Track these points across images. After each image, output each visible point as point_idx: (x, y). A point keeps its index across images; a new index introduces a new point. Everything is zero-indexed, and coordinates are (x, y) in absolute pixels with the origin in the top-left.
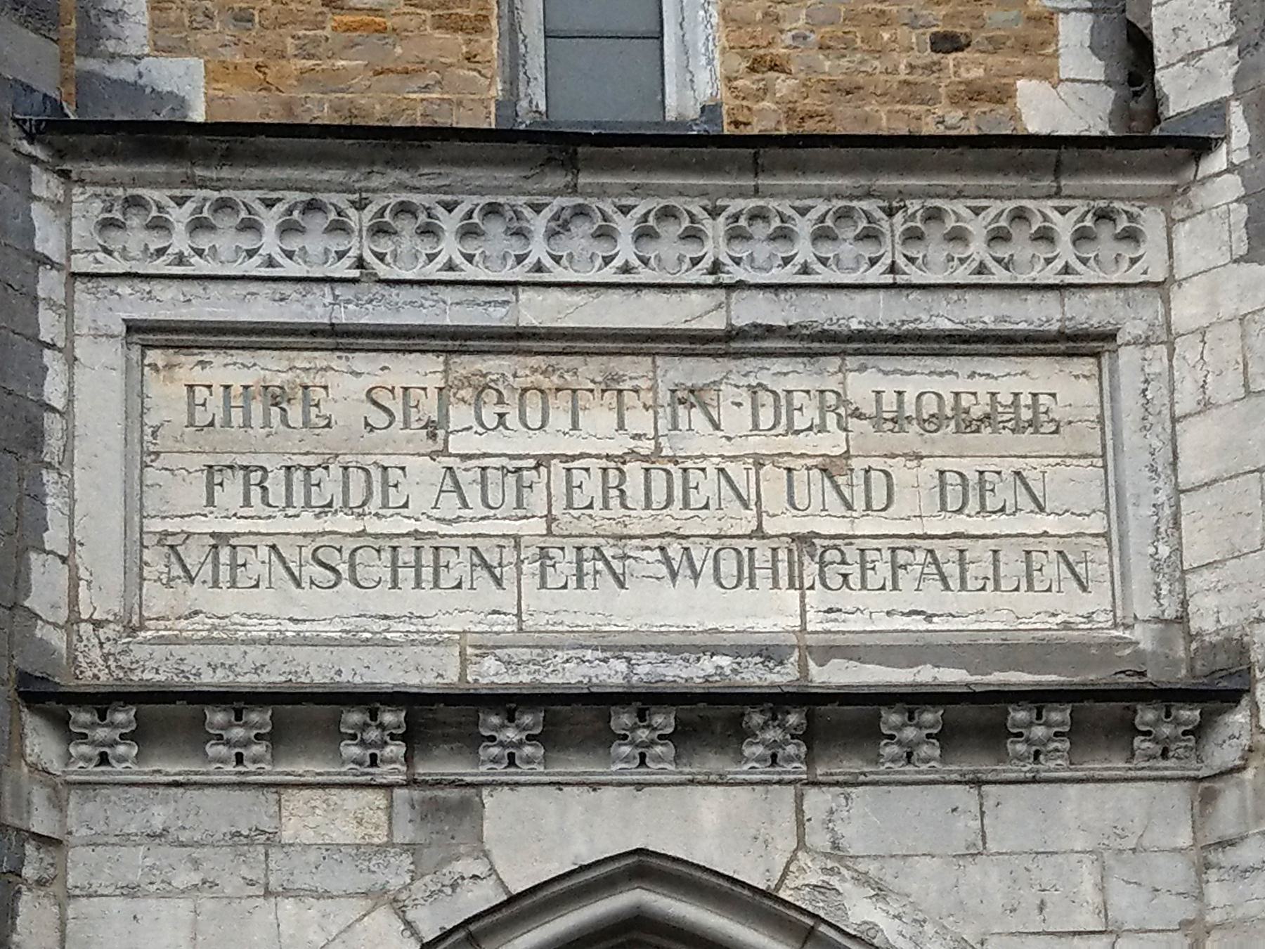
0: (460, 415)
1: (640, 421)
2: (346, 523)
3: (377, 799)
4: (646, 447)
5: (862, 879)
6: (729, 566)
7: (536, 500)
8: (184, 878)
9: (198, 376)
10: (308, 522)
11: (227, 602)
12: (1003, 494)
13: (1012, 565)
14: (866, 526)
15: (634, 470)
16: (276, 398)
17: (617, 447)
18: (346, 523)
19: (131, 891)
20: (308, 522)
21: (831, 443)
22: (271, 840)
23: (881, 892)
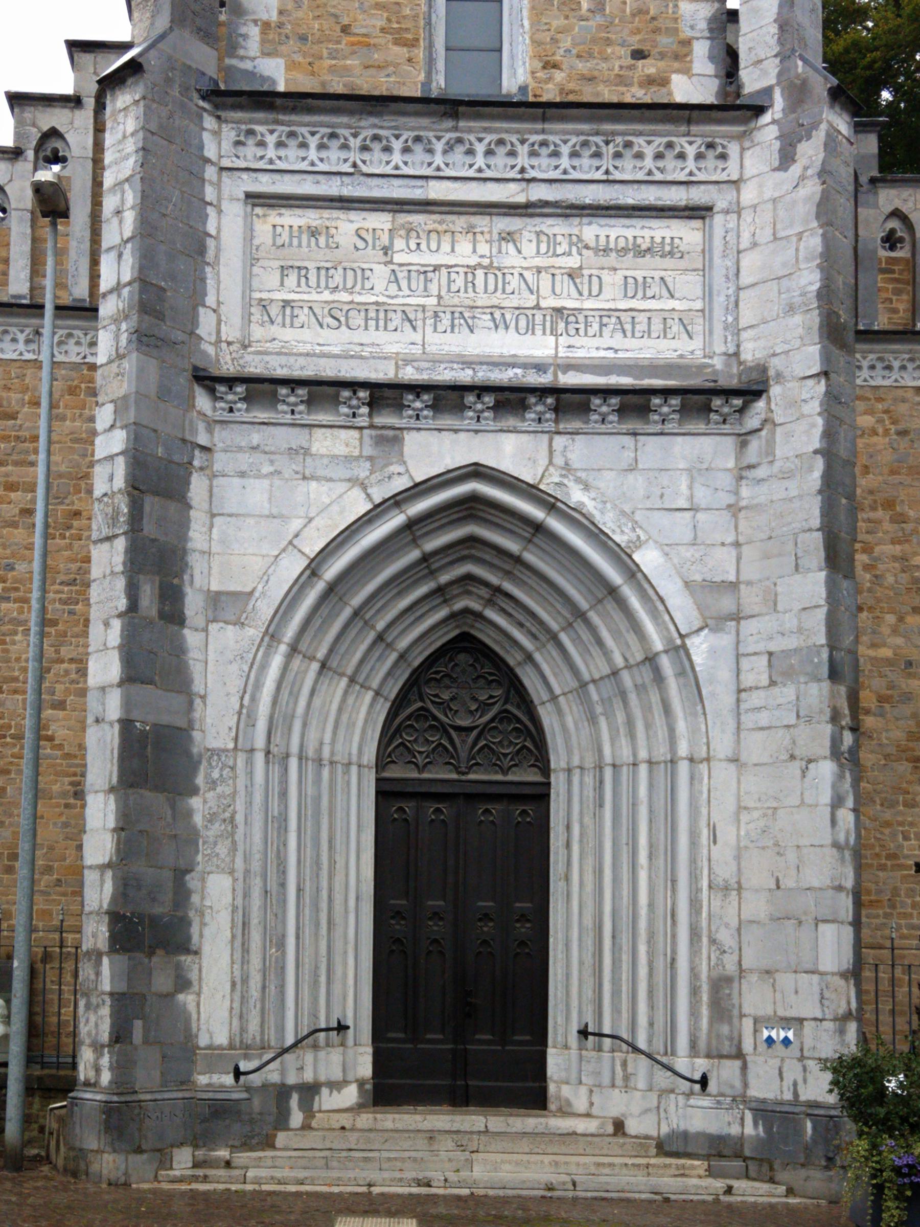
0: (399, 244)
1: (483, 248)
2: (344, 297)
3: (355, 434)
4: (486, 262)
5: (578, 480)
6: (523, 323)
7: (433, 288)
8: (266, 469)
9: (278, 221)
10: (327, 296)
11: (288, 334)
12: (655, 289)
13: (657, 326)
14: (589, 304)
15: (480, 273)
16: (314, 233)
17: (473, 261)
18: (344, 297)
19: (242, 475)
20: (327, 296)
21: (573, 262)
22: (306, 452)
23: (587, 487)
